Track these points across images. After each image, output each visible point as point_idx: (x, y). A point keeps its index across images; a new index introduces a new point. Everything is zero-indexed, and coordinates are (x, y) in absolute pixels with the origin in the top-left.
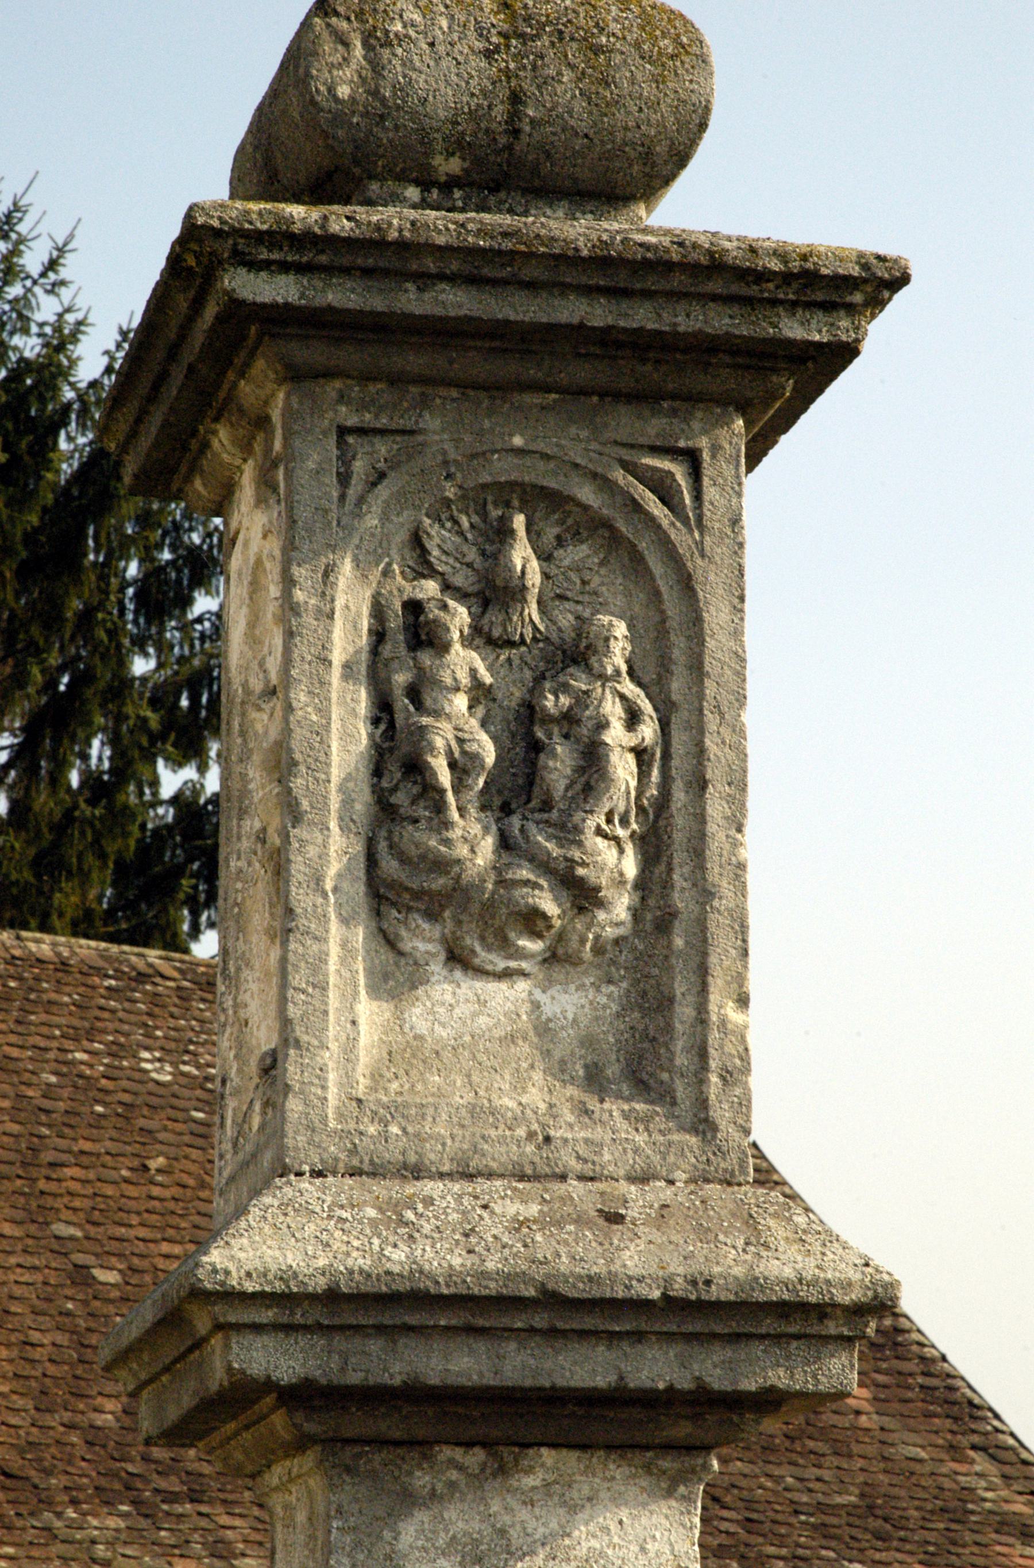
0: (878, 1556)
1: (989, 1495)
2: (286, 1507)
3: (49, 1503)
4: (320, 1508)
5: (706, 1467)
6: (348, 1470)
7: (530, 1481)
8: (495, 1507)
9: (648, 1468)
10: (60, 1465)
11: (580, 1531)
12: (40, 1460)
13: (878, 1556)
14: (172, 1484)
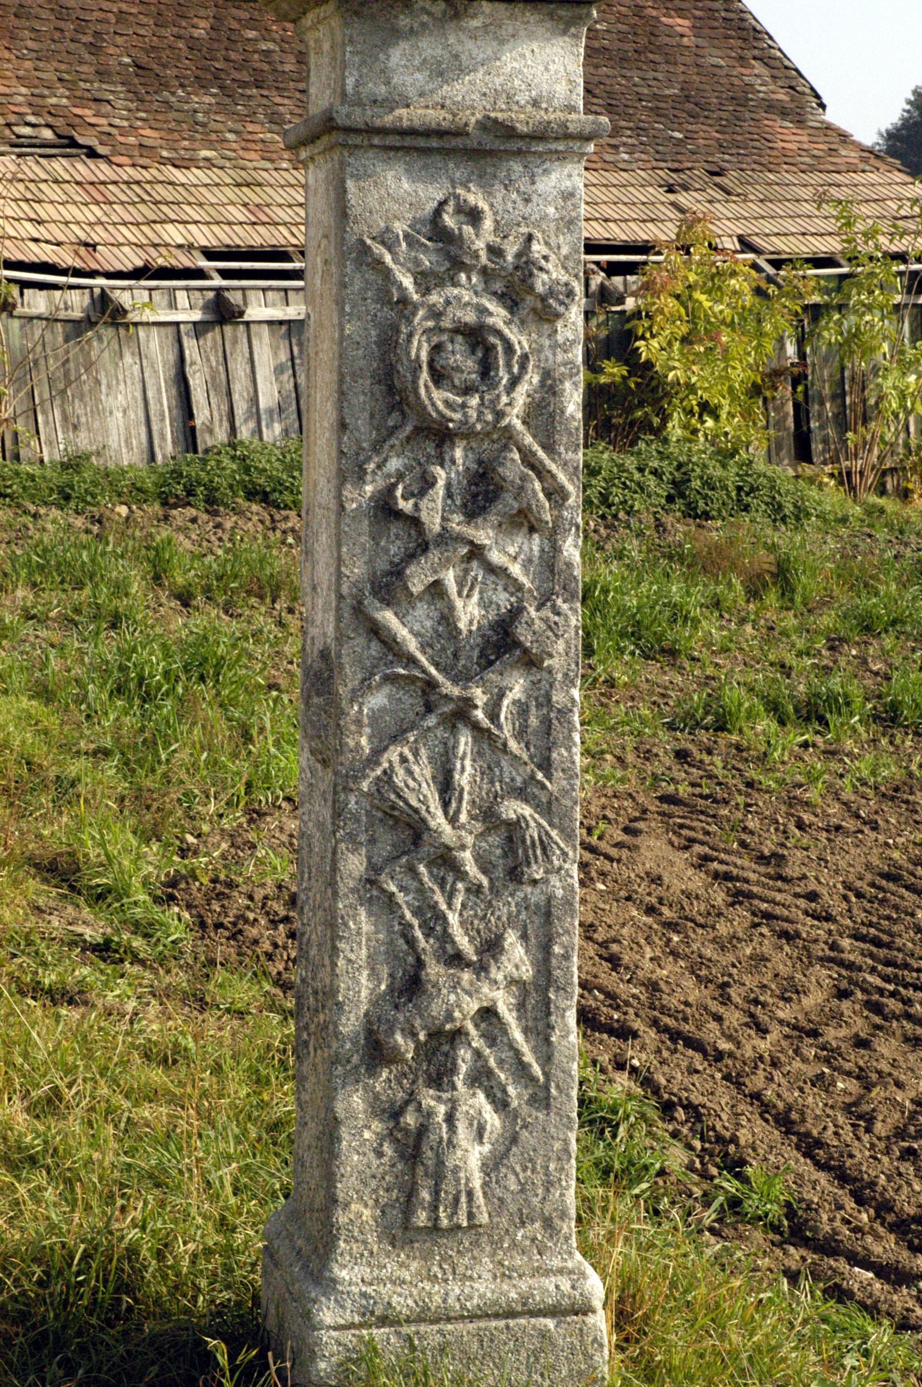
0: (690, 127)
1: (763, 88)
2: (317, 41)
3: (166, 86)
4: (339, 38)
5: (589, 15)
6: (356, 13)
7: (475, 23)
8: (452, 40)
9: (551, 16)
10: (173, 62)
11: (506, 57)
12: (160, 58)
13: (690, 127)
14: (245, 76)
